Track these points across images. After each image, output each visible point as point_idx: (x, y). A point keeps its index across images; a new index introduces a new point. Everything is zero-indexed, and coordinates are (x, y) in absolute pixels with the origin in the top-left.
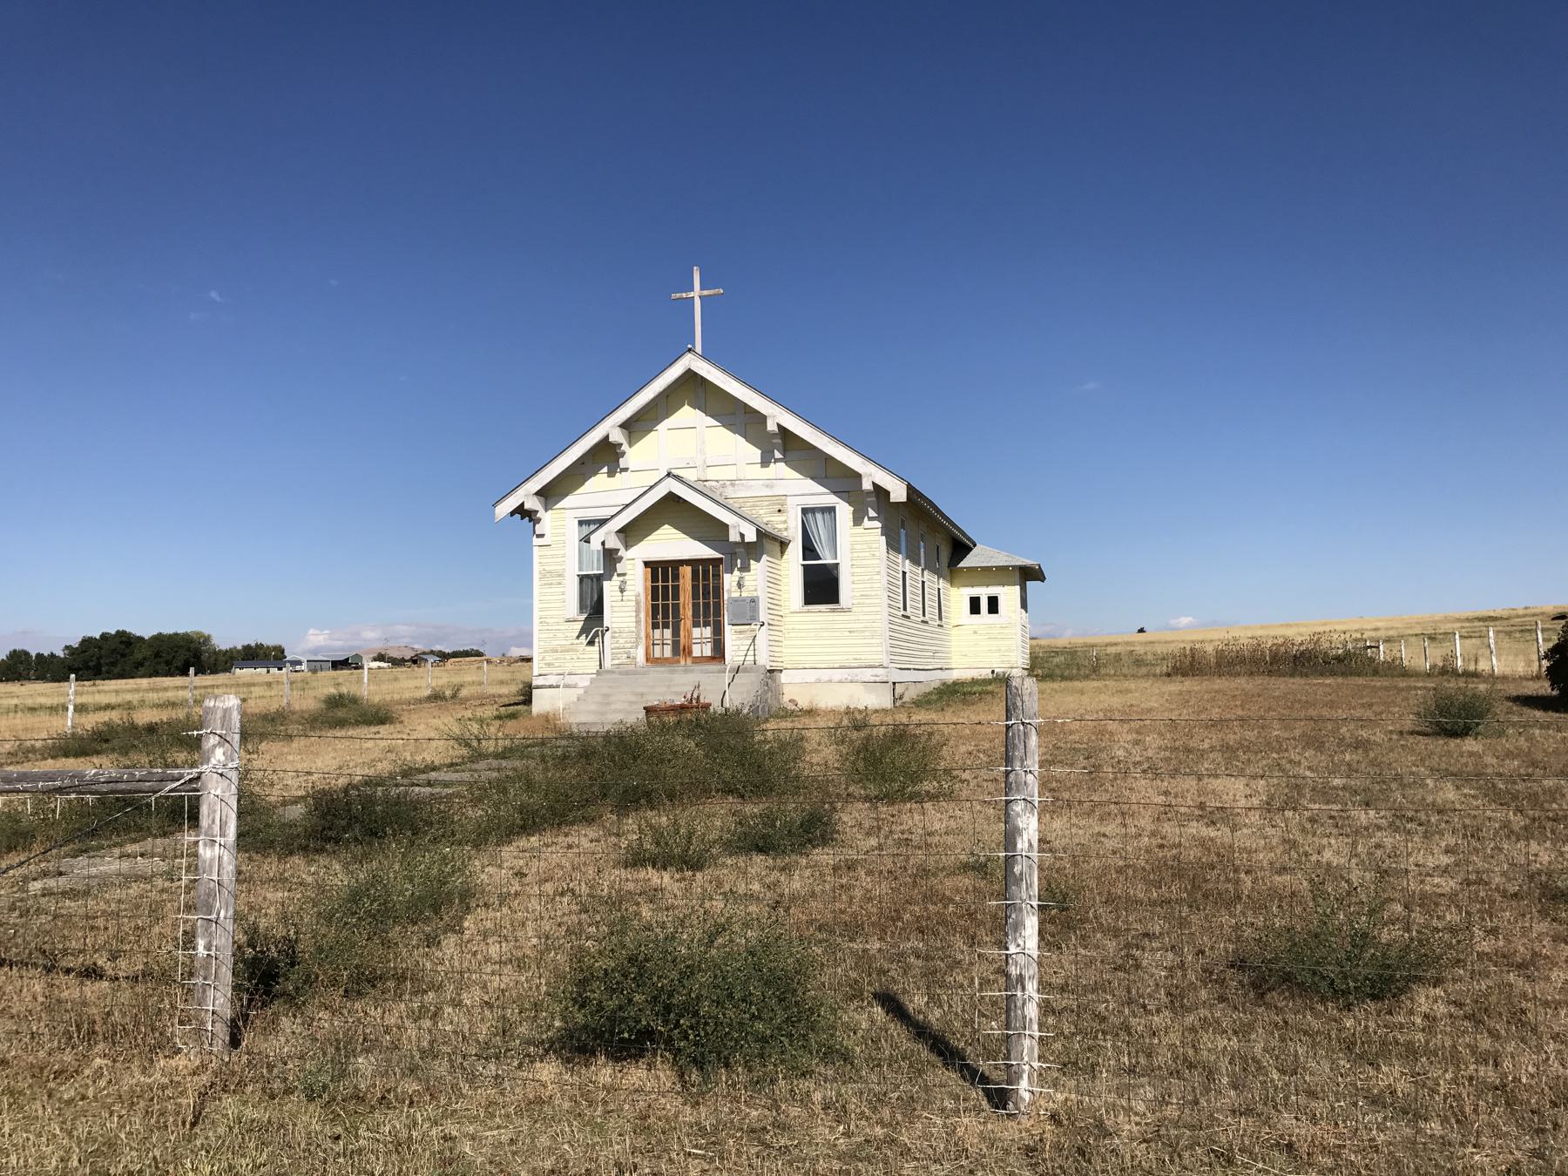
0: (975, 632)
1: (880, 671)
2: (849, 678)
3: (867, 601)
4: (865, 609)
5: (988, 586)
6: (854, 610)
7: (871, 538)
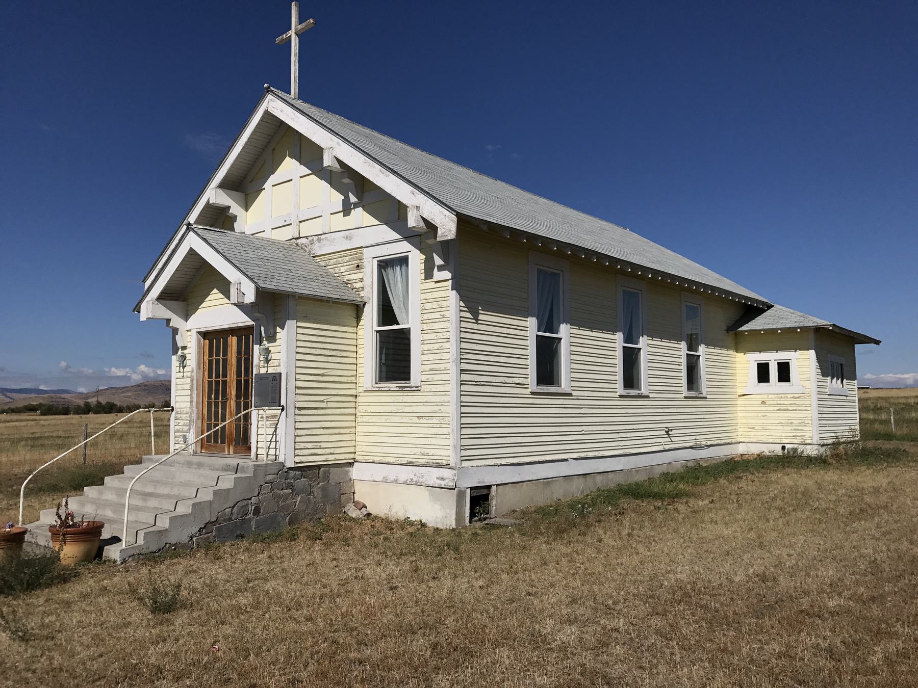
0: (763, 403)
1: (447, 473)
2: (415, 479)
3: (436, 377)
4: (434, 388)
5: (760, 352)
6: (423, 388)
7: (443, 294)
